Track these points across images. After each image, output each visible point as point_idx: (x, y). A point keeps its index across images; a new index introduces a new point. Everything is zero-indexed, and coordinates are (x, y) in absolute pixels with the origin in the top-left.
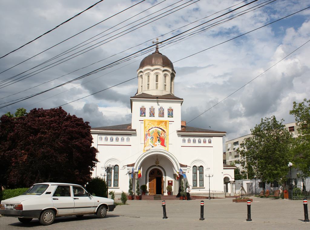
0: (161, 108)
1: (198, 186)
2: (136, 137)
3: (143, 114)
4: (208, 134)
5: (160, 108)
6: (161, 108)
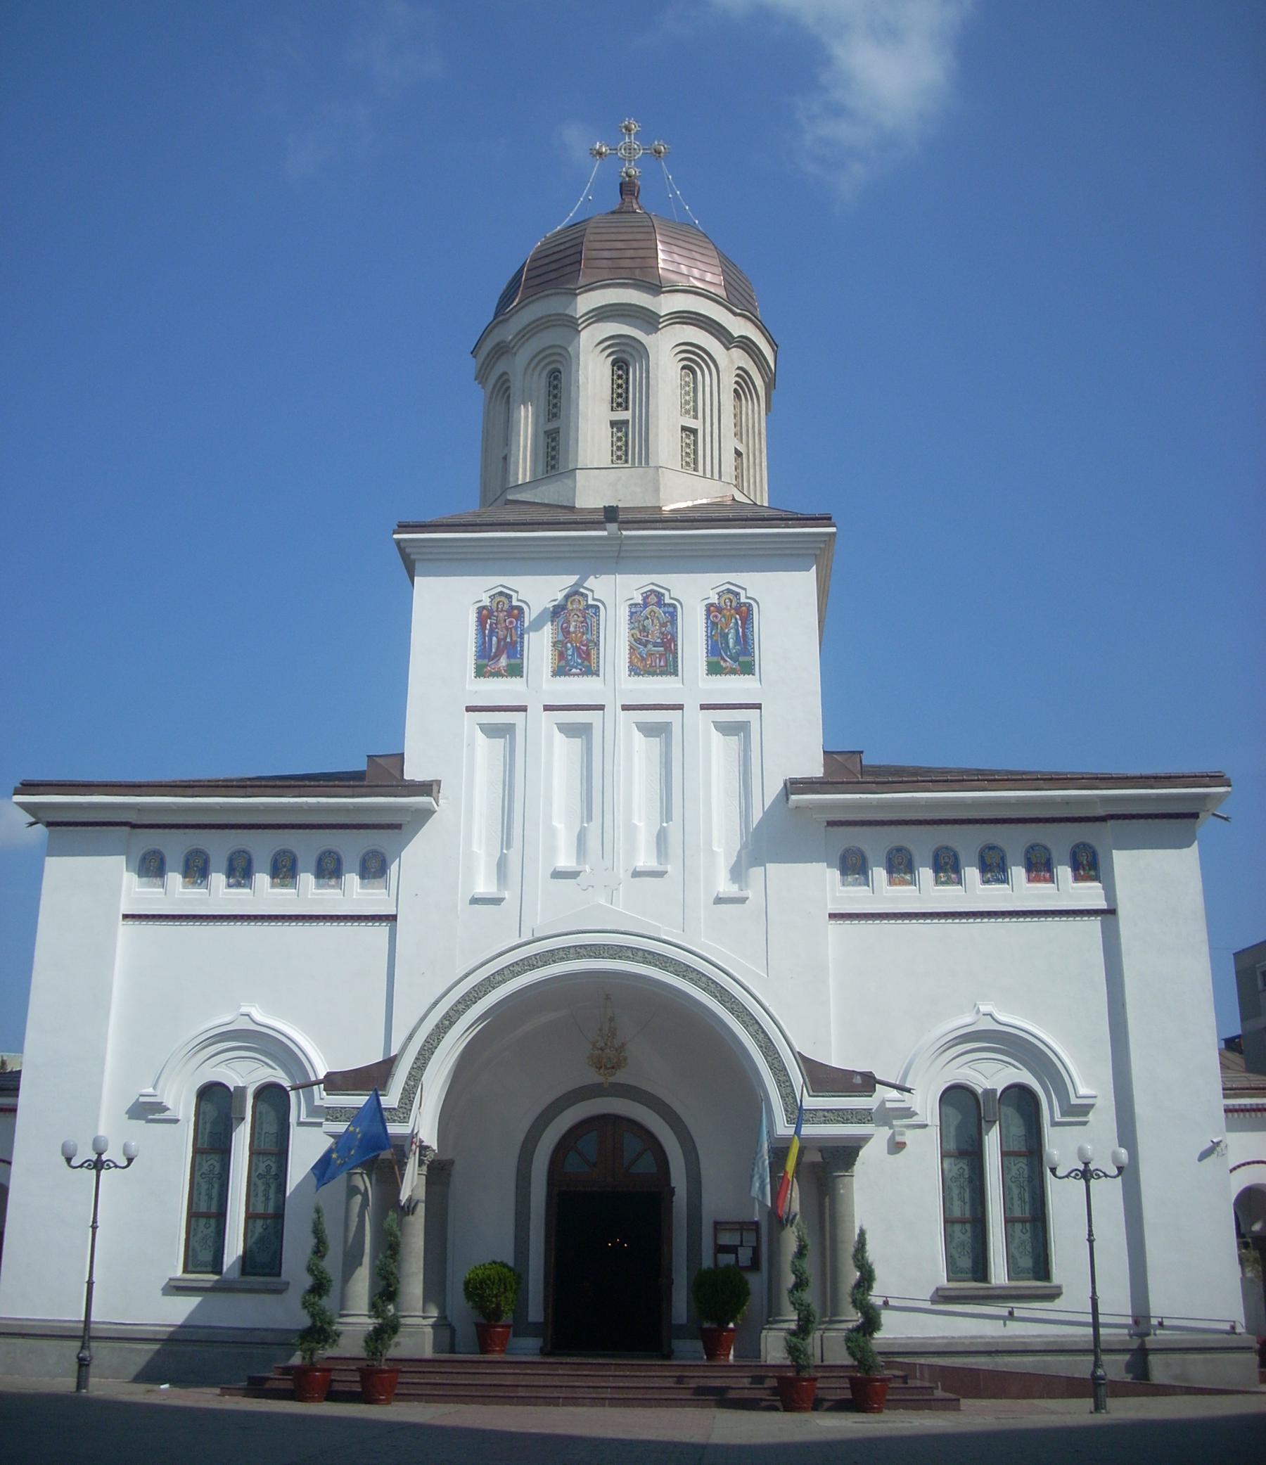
0: (646, 605)
1: (999, 1273)
2: (886, 1151)
3: (497, 656)
4: (1067, 802)
5: (639, 600)
6: (653, 599)
